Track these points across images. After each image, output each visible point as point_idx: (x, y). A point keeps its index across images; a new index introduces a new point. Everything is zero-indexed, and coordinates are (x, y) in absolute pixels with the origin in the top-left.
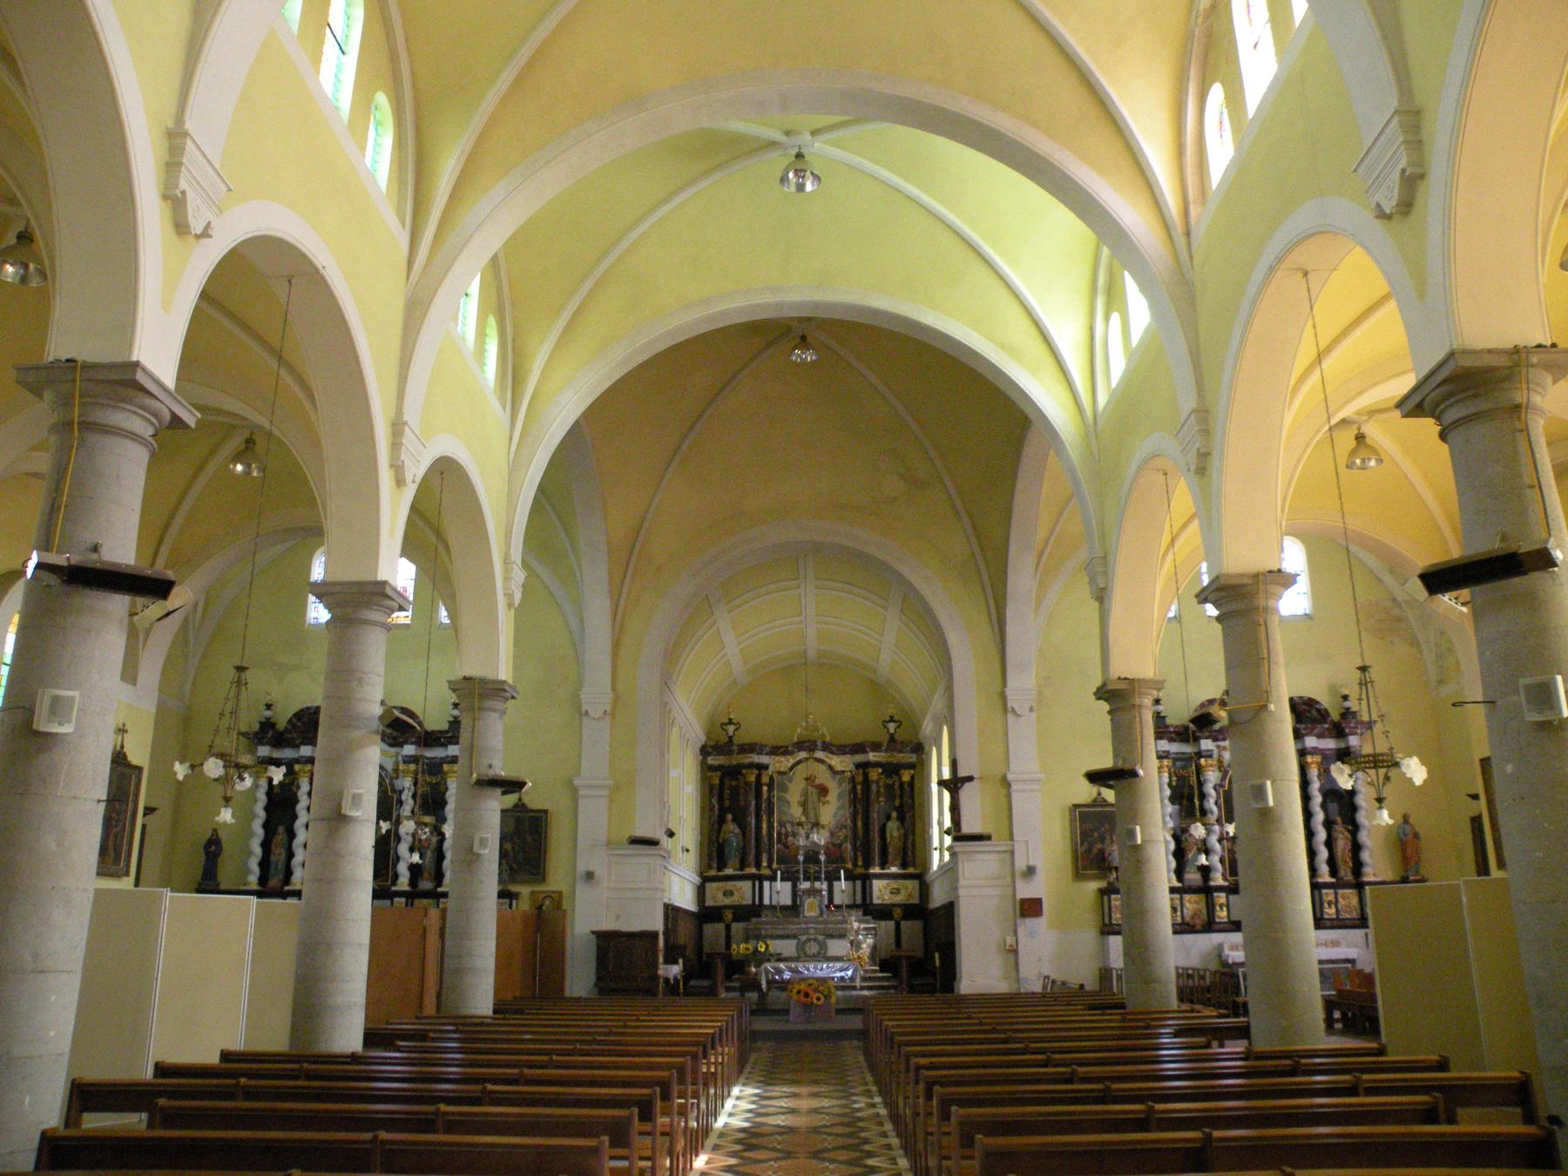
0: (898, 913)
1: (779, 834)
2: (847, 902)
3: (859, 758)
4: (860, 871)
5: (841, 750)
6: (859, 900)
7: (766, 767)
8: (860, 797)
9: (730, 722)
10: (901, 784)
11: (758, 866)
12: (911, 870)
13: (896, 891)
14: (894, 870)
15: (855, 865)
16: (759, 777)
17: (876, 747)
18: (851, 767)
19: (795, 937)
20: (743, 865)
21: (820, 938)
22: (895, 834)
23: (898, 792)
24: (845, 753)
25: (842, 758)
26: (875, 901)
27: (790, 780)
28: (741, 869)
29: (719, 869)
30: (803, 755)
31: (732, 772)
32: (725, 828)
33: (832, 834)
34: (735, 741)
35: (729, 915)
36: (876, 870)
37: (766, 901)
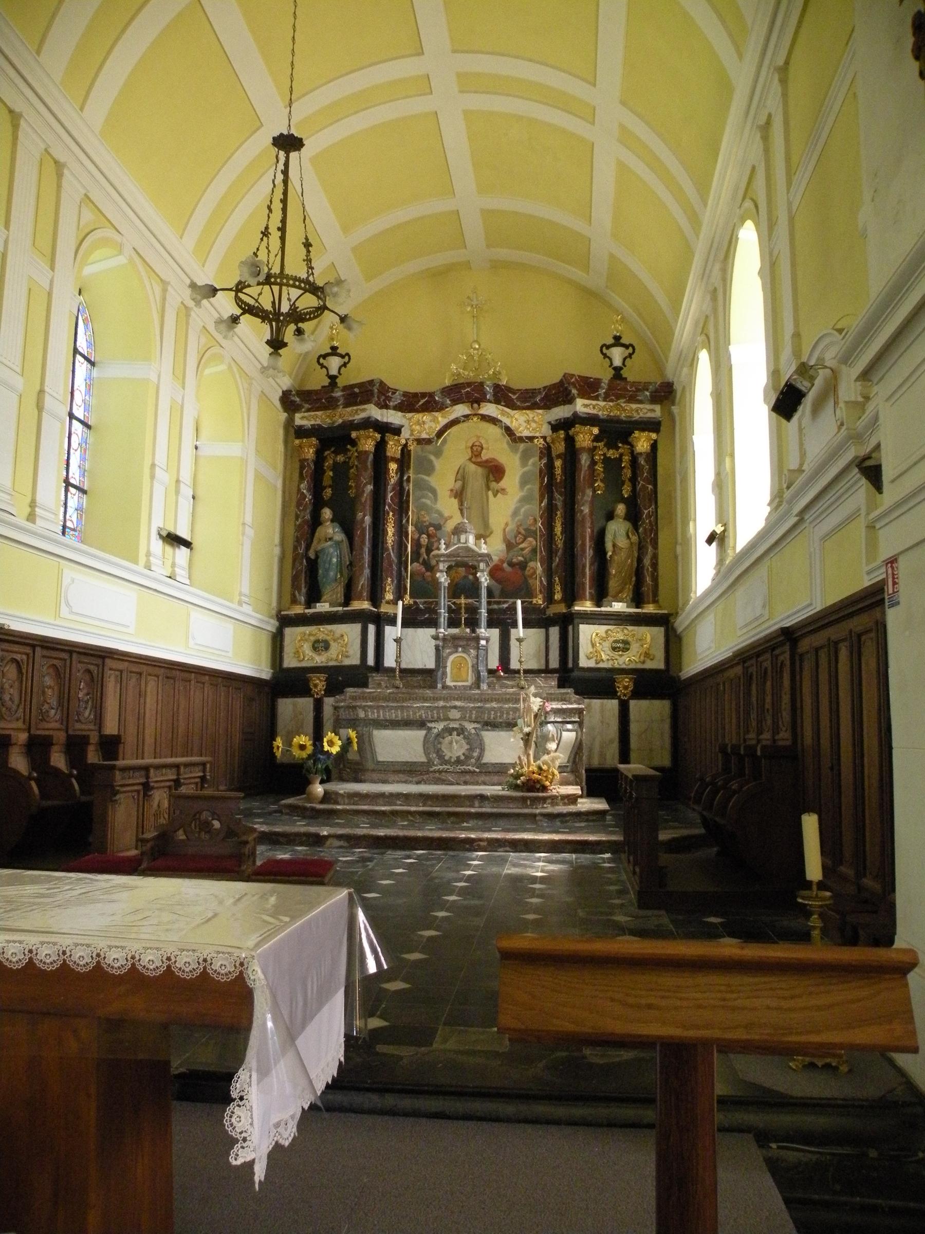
0: (624, 684)
1: (417, 544)
2: (533, 665)
3: (561, 412)
4: (562, 609)
5: (527, 399)
6: (554, 663)
7: (397, 431)
8: (560, 480)
9: (334, 351)
10: (634, 458)
11: (375, 597)
12: (650, 609)
13: (623, 646)
14: (618, 607)
15: (550, 599)
16: (381, 446)
17: (589, 387)
18: (546, 430)
19: (421, 724)
21: (470, 727)
22: (623, 543)
23: (628, 473)
24: (534, 407)
25: (531, 414)
26: (583, 662)
27: (438, 453)
28: (347, 603)
29: (309, 604)
30: (461, 410)
31: (335, 440)
32: (320, 532)
33: (510, 546)
34: (341, 382)
35: (319, 683)
36: (587, 606)
37: (389, 661)
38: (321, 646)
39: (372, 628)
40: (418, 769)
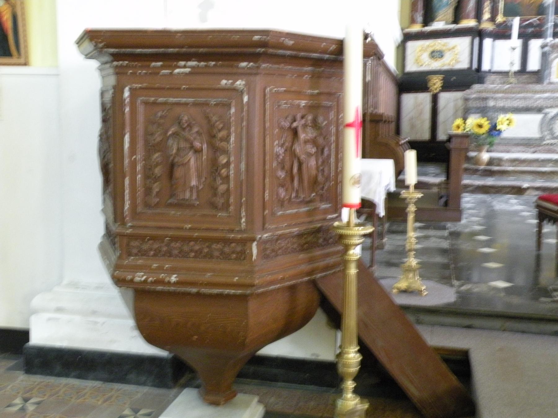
11: (478, 16)
19: (539, 110)
20: (458, 14)
28: (456, 21)
35: (436, 83)
37: (485, 67)
38: (436, 55)
39: (477, 41)
40: (534, 142)
